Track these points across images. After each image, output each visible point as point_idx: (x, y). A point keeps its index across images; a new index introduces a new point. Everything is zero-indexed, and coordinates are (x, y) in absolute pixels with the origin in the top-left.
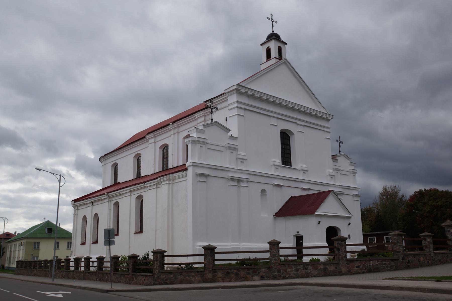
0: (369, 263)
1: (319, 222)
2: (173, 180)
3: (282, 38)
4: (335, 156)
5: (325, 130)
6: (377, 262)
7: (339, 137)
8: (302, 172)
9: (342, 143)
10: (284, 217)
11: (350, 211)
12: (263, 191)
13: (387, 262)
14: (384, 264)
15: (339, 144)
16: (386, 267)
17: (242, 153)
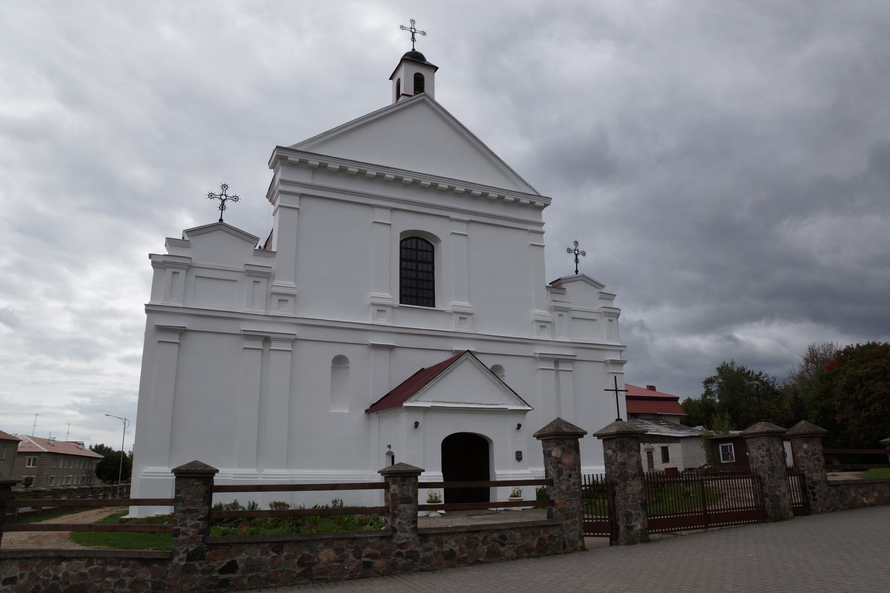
0: (54, 566)
1: (519, 426)
3: (430, 59)
4: (559, 282)
5: (530, 227)
6: (86, 566)
7: (576, 243)
8: (456, 318)
9: (584, 254)
10: (377, 413)
11: (522, 398)
12: (340, 361)
13: (124, 566)
14: (112, 574)
15: (220, 202)
16: (117, 584)
17: (282, 283)
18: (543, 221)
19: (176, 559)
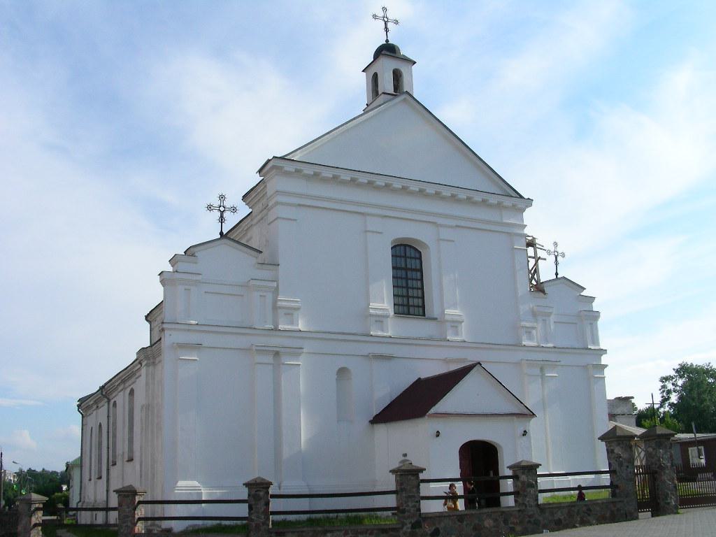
2: (154, 358)
7: (556, 244)
12: (342, 372)
15: (219, 214)
18: (525, 224)
19: (405, 529)
